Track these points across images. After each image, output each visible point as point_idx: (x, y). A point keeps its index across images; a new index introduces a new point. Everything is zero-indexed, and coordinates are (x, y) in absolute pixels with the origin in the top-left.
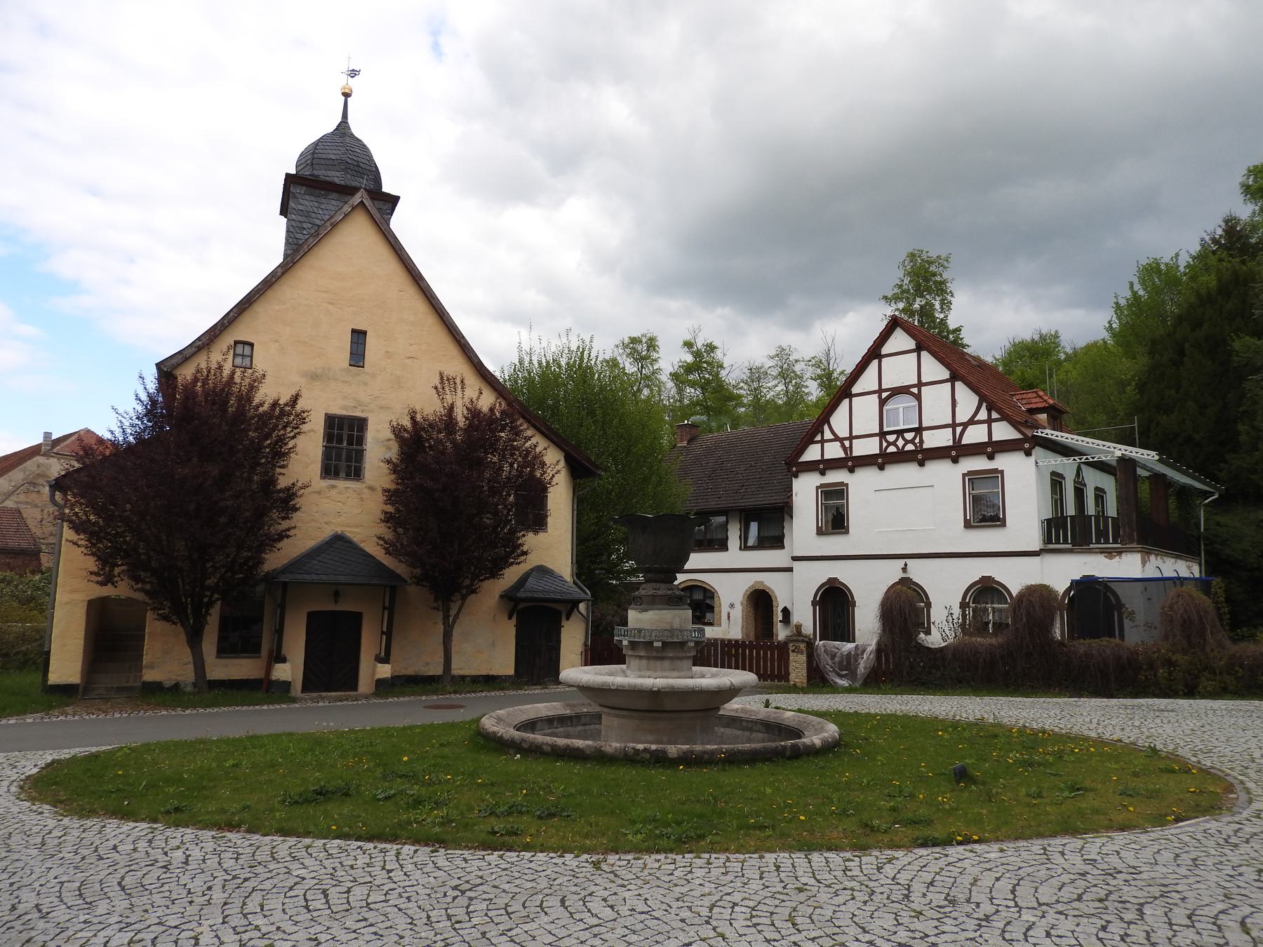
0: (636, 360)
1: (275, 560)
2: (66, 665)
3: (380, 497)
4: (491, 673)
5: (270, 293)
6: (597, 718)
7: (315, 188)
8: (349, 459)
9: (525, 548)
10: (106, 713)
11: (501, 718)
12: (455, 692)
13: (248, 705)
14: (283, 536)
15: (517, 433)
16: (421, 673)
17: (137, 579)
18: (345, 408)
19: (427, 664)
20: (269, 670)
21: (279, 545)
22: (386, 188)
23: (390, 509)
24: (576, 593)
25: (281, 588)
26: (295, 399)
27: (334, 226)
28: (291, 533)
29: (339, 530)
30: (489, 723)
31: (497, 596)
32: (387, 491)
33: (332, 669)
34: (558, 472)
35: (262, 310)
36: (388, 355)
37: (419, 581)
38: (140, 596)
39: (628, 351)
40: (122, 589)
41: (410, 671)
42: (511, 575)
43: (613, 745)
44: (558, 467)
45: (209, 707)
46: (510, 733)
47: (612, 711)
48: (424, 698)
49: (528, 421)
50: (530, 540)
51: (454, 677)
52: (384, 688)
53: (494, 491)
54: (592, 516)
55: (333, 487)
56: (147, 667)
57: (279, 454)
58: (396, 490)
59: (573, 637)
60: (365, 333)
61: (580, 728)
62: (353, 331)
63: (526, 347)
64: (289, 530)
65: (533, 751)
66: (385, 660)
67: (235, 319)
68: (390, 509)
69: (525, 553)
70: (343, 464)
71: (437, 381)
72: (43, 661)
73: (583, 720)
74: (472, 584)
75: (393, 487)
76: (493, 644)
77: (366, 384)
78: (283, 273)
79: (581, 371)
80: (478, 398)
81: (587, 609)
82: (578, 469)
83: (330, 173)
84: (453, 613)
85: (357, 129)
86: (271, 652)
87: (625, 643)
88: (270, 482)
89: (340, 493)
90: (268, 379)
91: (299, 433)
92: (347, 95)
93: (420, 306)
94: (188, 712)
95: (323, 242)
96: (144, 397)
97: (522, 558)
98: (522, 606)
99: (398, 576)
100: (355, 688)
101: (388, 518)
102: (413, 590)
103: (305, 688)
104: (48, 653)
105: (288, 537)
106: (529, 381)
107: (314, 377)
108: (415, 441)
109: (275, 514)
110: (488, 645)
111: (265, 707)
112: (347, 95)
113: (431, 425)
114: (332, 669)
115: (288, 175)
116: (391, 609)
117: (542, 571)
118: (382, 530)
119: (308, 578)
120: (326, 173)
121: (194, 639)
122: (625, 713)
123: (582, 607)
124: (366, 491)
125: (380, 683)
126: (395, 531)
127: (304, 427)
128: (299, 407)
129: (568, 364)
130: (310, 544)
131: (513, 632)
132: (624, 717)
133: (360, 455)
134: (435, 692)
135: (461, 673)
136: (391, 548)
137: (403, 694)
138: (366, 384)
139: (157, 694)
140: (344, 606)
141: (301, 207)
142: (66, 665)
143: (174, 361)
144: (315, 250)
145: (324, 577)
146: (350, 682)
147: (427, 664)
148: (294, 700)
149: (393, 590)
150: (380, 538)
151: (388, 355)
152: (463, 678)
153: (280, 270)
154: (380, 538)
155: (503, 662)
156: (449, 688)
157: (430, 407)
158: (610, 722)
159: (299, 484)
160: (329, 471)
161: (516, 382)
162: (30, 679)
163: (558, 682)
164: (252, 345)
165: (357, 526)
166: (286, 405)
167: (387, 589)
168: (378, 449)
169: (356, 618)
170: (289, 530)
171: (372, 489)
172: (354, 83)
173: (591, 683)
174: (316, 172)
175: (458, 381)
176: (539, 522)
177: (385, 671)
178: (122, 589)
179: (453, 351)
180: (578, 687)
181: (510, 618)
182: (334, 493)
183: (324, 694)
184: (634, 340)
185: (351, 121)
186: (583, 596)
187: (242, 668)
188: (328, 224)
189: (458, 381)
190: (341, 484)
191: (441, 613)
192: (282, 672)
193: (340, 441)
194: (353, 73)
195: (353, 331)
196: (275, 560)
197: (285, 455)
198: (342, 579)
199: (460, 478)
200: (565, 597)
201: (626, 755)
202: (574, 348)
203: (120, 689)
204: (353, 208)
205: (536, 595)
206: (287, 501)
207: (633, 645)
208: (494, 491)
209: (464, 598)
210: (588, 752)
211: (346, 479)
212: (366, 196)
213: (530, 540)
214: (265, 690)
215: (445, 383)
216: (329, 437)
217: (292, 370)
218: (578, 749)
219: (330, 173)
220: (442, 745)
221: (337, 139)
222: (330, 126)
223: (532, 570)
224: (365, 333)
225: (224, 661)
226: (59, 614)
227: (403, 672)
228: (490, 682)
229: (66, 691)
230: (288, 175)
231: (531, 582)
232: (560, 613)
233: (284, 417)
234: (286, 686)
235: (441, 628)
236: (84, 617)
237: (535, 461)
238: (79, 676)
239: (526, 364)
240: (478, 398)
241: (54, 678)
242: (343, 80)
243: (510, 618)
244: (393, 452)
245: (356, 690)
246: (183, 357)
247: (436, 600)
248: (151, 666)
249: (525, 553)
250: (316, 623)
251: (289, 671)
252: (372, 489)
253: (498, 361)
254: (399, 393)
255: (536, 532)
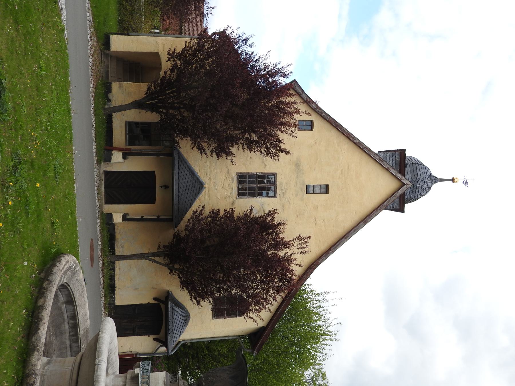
0: (313, 378)
1: (186, 148)
2: (120, 43)
3: (228, 207)
4: (117, 289)
5: (343, 137)
6: (74, 353)
7: (400, 166)
8: (250, 189)
9: (202, 303)
10: (93, 55)
11: (74, 271)
12: (103, 264)
13: (96, 134)
14: (202, 150)
15: (278, 290)
16: (116, 243)
17: (172, 70)
18: (281, 184)
19: (123, 247)
20: (119, 149)
21: (195, 148)
22: (407, 206)
23: (222, 213)
24: (172, 343)
25: (170, 155)
26: (284, 151)
27: (387, 170)
28: (204, 155)
29: (206, 186)
30: (68, 261)
31: (168, 289)
32: (233, 212)
33: (119, 188)
34: (255, 321)
35: (333, 133)
36: (316, 207)
37: (177, 236)
38: (162, 74)
39: (317, 372)
40: (166, 65)
41: (118, 236)
42: (183, 296)
43: (39, 362)
44: (258, 320)
45: (95, 111)
46: (58, 277)
47: (77, 364)
48: (99, 243)
49: (286, 297)
50: (207, 306)
51: (114, 263)
52: (107, 220)
53: (238, 279)
54: (225, 350)
55: (233, 180)
56: (120, 85)
57: (250, 145)
58: (233, 217)
59: (141, 344)
60: (327, 192)
61: (68, 343)
62: (327, 186)
63: (328, 297)
64: (206, 153)
65: (40, 288)
66: (125, 218)
67: (325, 119)
68: (222, 213)
69: (198, 303)
70: (247, 186)
71: (303, 235)
72: (124, 31)
73: (74, 345)
74: (176, 270)
75: (236, 214)
76: (136, 289)
77: (297, 195)
78: (355, 143)
79: (316, 336)
80: (297, 265)
81: (162, 353)
82: (256, 337)
83: (409, 173)
84: (157, 259)
85: (435, 187)
86: (129, 150)
87: (137, 371)
88: (233, 140)
89: (229, 185)
90: (293, 139)
91: (264, 155)
92: (453, 180)
93: (348, 224)
94: (92, 99)
95: (378, 165)
96: (279, 66)
97: (195, 301)
98: (163, 306)
99: (179, 223)
100: (107, 203)
101: (215, 213)
102: (171, 233)
103: (107, 173)
104: (128, 35)
105: (201, 153)
106: (306, 302)
107: (297, 165)
108: (265, 228)
109: (214, 145)
110: (136, 285)
111: (94, 143)
112: (453, 180)
113: (277, 234)
114: (119, 188)
115: (404, 151)
116: (158, 219)
117: (186, 318)
118: (207, 212)
119: (176, 167)
120: (409, 171)
121: (138, 105)
122: (75, 377)
123: (163, 349)
124: (231, 200)
125: (110, 216)
126: (209, 216)
127: (268, 158)
128: (281, 154)
129: (319, 326)
130: (197, 170)
131: (145, 301)
132: (72, 375)
133: (253, 194)
134: (103, 250)
135: (117, 269)
136: (198, 214)
137: (102, 229)
138: (297, 195)
139: (104, 90)
140: (159, 193)
141: (388, 159)
142: (120, 43)
143: (298, 88)
144: (372, 160)
145: (176, 177)
146: (110, 200)
147: (123, 247)
148: (99, 162)
149: (171, 220)
150: (203, 207)
151: (316, 207)
152: (114, 269)
153: (357, 141)
154: (203, 207)
155: (124, 297)
156: (106, 260)
157: (288, 234)
158: (69, 362)
159: (233, 158)
160: (242, 178)
161: (304, 293)
162: (113, 22)
163: (105, 316)
164: (312, 129)
165: (209, 196)
166: (280, 147)
167: (170, 218)
168: (259, 205)
169: (151, 200)
170: (206, 153)
171: (233, 203)
172: (460, 183)
173: (101, 341)
174: (408, 166)
175: (306, 249)
176: (220, 311)
177: (118, 219)
178: (166, 65)
179: (324, 247)
180: (98, 335)
181: (154, 299)
182: (229, 181)
183: (103, 182)
184: (324, 375)
185: (439, 183)
186: (171, 348)
187: (119, 135)
188: (388, 166)
189: (306, 249)
190: (235, 185)
191: (156, 251)
192: (117, 157)
193: (260, 183)
194: (466, 183)
195: (327, 186)
196: (186, 148)
197: (250, 149)
198: (176, 187)
199: (243, 259)
200: (169, 338)
201: (28, 376)
202: (330, 329)
203: (107, 72)
204: (400, 180)
205: (170, 314)
206: (222, 150)
207: (135, 378)
208: (238, 279)
209: (166, 265)
210: (34, 338)
211: (238, 188)
212: (408, 186)
213: (207, 306)
214: (106, 148)
215: (304, 240)
216: (263, 176)
217: (299, 156)
218: (37, 329)
219: (409, 173)
220: (53, 223)
221: (429, 176)
222: (434, 173)
223: (187, 311)
224: (327, 192)
225: (124, 125)
226: (151, 39)
227: (117, 232)
228: (111, 288)
229: (107, 43)
230: (404, 151)
231: (179, 311)
232: (158, 333)
233: (272, 147)
234: (108, 159)
235: (146, 252)
236: (148, 51)
237: (260, 302)
238: (115, 50)
239: (317, 298)
240: (297, 265)
241: (114, 38)
242: (460, 177)
243: (154, 299)
244: (256, 214)
245: (106, 203)
246: (300, 93)
247: (165, 247)
248: (120, 87)
249: (198, 303)
250: (148, 177)
251: (118, 162)
252: (233, 203)
253: (315, 282)
254: (294, 214)
255: (213, 309)
